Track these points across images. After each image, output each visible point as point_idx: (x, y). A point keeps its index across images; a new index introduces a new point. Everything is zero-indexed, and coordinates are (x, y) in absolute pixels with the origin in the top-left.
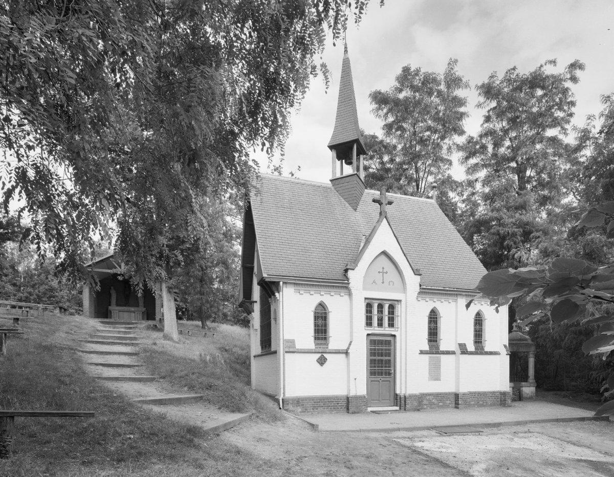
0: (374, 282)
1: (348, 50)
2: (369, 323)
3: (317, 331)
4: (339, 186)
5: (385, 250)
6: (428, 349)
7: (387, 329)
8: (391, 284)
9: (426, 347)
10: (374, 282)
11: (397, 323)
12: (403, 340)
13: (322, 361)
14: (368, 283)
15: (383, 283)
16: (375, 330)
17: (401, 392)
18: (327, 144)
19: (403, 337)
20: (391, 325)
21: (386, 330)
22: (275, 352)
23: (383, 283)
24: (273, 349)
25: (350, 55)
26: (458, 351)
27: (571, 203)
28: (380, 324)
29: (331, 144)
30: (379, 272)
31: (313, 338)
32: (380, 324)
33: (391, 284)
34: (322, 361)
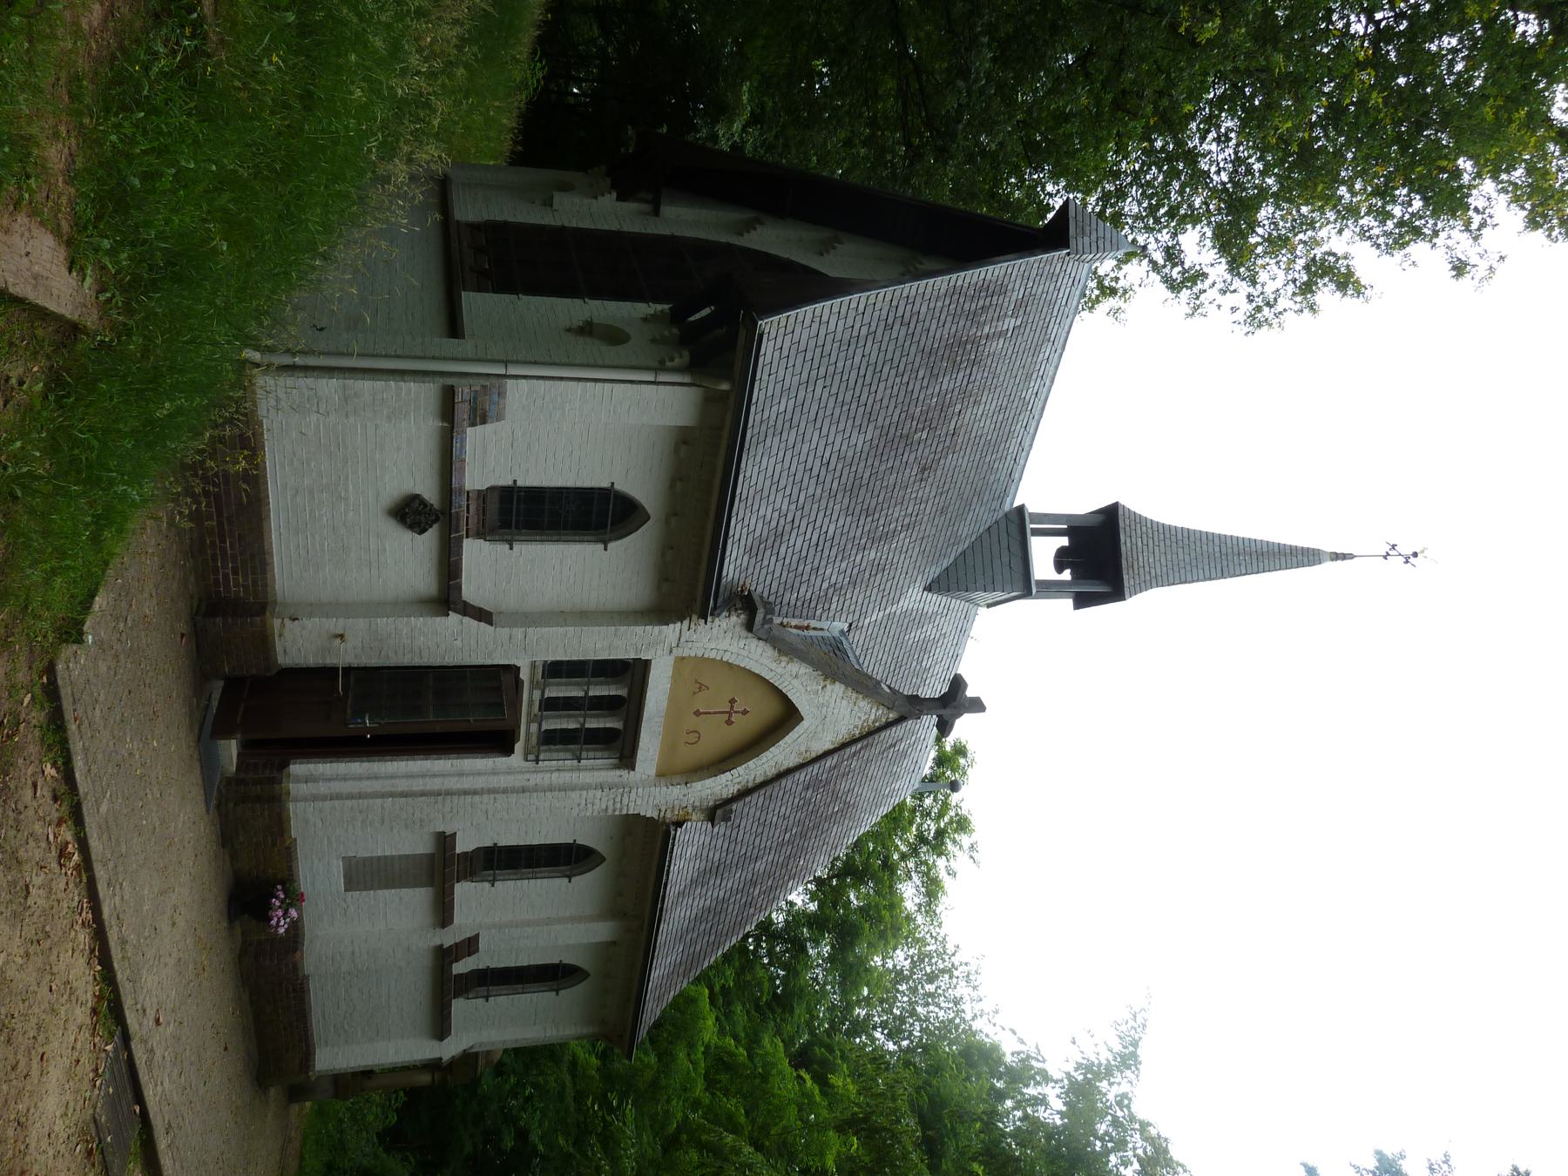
0: (701, 687)
1: (1339, 562)
2: (556, 670)
3: (536, 496)
4: (1004, 536)
5: (802, 719)
6: (458, 851)
7: (537, 695)
8: (692, 738)
9: (463, 845)
10: (701, 687)
11: (555, 755)
12: (494, 782)
13: (410, 513)
14: (693, 671)
15: (697, 713)
16: (530, 698)
17: (298, 780)
18: (1122, 502)
19: (503, 781)
20: (551, 739)
21: (527, 730)
22: (454, 328)
23: (697, 713)
24: (472, 302)
25: (1328, 566)
26: (449, 938)
27: (721, 110)
28: (550, 705)
29: (1120, 512)
30: (732, 701)
31: (506, 481)
32: (550, 705)
33: (692, 738)
34: (410, 513)
